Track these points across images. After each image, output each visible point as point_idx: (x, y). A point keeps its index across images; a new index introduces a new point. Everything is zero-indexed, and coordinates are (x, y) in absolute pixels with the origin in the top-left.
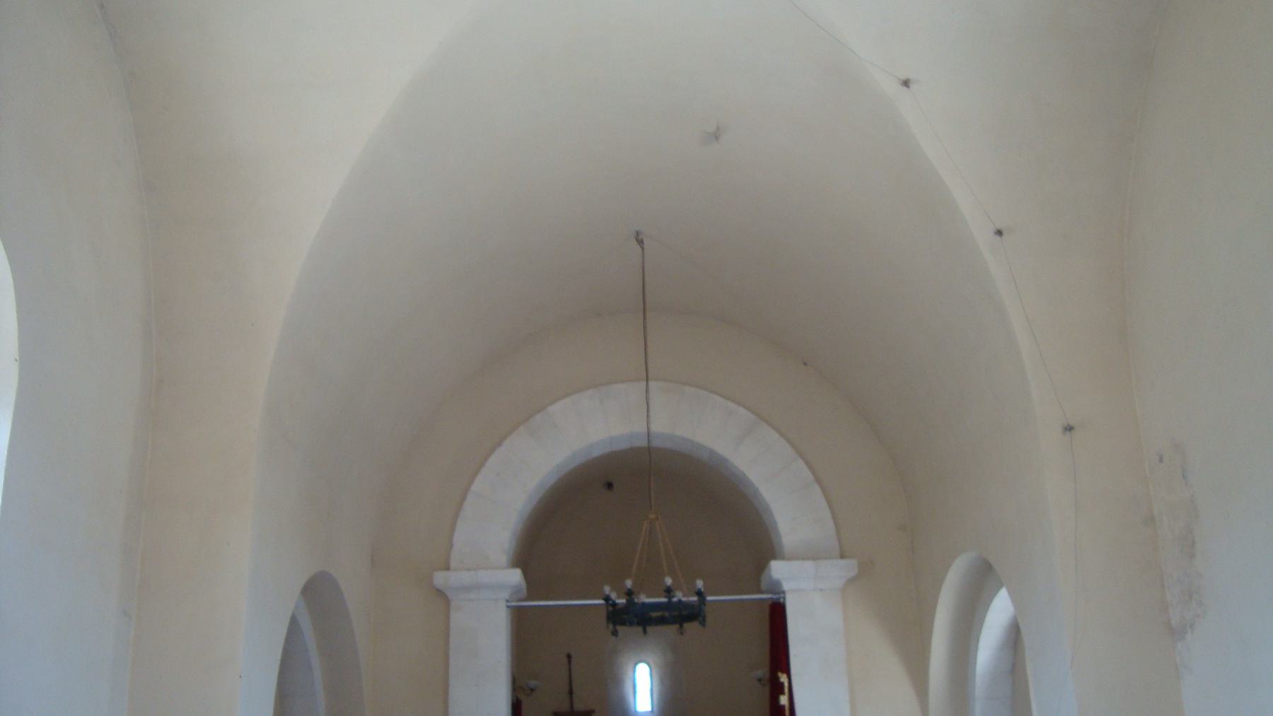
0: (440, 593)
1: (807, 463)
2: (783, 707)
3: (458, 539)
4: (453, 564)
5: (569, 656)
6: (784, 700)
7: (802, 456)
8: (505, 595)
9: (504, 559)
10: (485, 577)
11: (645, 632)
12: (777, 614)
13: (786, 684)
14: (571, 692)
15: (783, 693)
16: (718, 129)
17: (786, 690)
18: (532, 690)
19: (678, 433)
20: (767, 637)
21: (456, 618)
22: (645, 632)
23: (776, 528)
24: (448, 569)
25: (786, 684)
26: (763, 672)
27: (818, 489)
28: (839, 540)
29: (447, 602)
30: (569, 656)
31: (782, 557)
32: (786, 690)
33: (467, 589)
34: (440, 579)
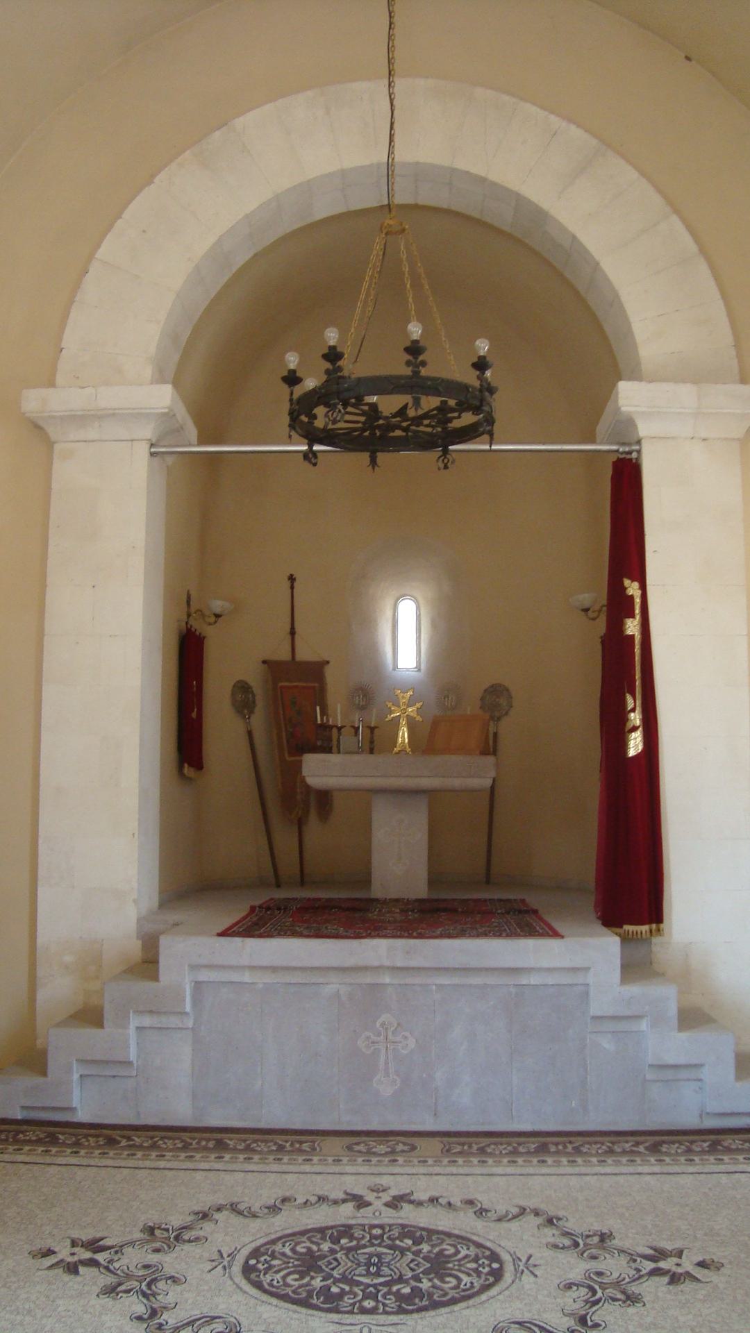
0: (37, 427)
1: (684, 221)
2: (632, 597)
3: (71, 339)
4: (59, 379)
5: (292, 579)
6: (632, 627)
7: (677, 211)
8: (147, 431)
9: (148, 372)
10: (112, 397)
11: (373, 462)
12: (626, 479)
13: (638, 601)
14: (293, 633)
15: (633, 616)
16: (663, 974)
17: (637, 611)
18: (218, 616)
19: (462, 164)
20: (679, 1128)
21: (66, 473)
22: (373, 462)
23: (629, 333)
24: (52, 384)
25: (638, 601)
26: (595, 595)
27: (703, 267)
28: (739, 356)
29: (49, 444)
30: (292, 579)
31: (636, 375)
32: (637, 611)
33: (81, 419)
34: (33, 401)
